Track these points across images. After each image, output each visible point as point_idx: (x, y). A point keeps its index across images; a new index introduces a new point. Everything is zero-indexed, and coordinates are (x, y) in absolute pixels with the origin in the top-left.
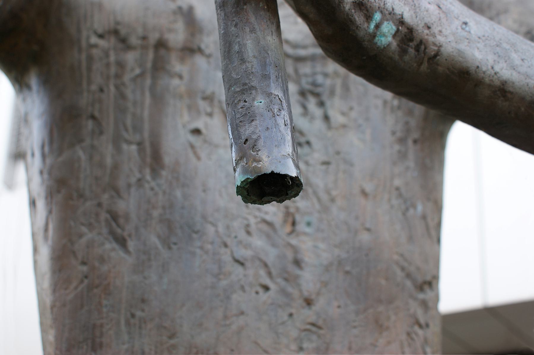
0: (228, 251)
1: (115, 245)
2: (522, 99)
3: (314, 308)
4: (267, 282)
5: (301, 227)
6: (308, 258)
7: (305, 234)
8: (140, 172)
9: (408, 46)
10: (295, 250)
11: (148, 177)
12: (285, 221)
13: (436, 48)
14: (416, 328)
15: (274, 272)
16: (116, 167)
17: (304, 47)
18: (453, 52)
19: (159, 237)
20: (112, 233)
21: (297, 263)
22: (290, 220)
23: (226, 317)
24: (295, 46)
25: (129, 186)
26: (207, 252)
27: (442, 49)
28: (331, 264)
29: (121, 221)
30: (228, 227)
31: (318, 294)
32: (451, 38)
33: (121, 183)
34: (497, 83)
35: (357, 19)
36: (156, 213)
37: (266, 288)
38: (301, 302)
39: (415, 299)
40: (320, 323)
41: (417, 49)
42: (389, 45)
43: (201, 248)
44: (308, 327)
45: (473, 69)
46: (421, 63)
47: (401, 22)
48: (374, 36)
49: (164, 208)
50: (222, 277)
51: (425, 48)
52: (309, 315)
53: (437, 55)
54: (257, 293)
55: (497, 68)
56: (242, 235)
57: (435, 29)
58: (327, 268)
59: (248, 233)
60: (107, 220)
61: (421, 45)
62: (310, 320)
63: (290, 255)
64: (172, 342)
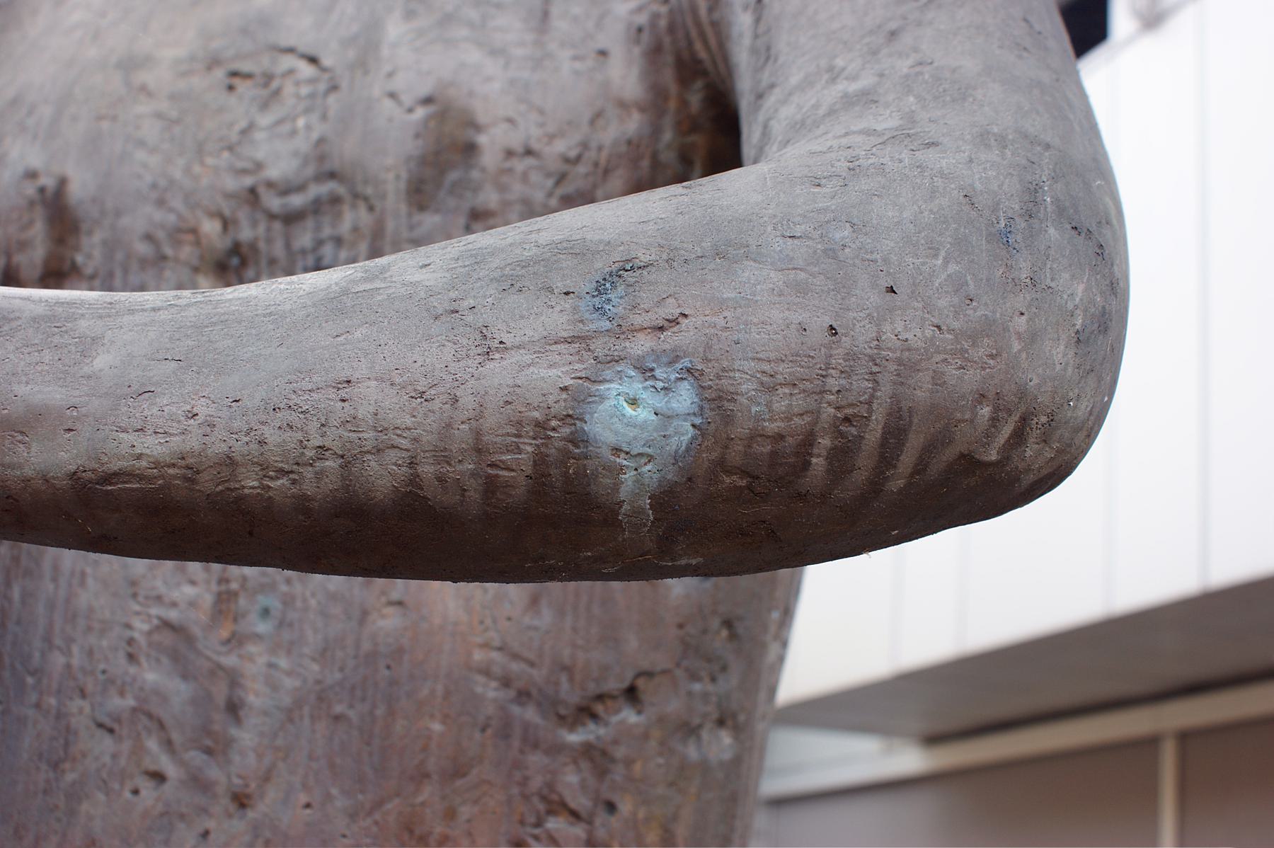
0: (86, 705)
3: (251, 814)
6: (256, 697)
7: (258, 637)
10: (234, 679)
15: (176, 736)
17: (301, 188)
22: (666, 324)
24: (286, 190)
28: (299, 704)
30: (90, 653)
31: (267, 778)
38: (225, 802)
43: (38, 706)
50: (67, 766)
54: (136, 792)
56: (120, 664)
58: (290, 715)
59: (131, 657)
63: (220, 692)
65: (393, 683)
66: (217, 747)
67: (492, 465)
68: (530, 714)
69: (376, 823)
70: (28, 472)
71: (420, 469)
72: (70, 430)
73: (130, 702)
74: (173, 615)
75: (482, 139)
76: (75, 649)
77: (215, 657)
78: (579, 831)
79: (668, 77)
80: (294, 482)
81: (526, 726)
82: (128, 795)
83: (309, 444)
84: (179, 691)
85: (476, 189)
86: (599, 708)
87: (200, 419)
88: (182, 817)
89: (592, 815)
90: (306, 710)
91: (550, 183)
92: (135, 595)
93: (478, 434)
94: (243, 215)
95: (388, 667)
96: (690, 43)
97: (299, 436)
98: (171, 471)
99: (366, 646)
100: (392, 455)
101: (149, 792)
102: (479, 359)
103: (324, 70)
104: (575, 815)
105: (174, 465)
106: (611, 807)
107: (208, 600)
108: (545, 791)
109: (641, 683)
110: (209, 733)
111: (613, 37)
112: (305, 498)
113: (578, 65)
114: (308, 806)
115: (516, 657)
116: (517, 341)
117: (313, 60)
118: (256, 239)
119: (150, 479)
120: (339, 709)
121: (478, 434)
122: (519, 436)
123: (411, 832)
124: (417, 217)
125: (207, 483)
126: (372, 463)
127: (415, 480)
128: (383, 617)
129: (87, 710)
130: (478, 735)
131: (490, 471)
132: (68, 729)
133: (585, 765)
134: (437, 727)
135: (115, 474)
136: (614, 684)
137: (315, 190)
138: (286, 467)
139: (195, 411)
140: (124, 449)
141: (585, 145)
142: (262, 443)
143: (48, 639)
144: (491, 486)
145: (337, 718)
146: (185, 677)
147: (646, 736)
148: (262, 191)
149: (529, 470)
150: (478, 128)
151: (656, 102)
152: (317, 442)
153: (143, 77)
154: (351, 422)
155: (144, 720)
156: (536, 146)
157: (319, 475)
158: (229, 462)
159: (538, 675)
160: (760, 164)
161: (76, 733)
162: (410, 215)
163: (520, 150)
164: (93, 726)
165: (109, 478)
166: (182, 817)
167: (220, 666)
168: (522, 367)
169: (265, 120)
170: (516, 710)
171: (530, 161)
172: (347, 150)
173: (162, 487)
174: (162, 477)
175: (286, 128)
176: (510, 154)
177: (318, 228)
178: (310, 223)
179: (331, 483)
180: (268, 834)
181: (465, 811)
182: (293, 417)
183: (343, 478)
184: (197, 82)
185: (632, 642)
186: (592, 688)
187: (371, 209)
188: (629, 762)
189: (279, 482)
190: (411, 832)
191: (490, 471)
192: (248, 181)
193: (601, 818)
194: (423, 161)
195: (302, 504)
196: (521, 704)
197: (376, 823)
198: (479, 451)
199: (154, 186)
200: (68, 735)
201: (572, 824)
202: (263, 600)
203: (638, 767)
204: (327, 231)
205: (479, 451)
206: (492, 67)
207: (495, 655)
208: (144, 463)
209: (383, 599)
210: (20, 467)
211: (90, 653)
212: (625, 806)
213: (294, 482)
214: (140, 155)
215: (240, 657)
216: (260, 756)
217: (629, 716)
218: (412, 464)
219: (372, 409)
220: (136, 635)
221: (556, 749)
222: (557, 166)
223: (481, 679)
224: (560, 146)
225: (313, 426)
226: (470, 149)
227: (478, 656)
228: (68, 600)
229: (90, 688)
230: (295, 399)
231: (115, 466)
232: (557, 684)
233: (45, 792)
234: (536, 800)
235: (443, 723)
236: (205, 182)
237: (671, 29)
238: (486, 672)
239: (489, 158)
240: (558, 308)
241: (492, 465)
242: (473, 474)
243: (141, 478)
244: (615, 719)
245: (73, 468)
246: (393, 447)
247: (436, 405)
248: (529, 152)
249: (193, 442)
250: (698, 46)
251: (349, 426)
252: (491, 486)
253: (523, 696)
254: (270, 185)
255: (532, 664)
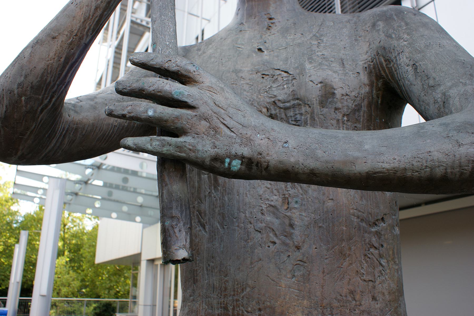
1: (201, 228)
2: (327, 175)
4: (275, 239)
5: (293, 205)
6: (297, 222)
8: (210, 189)
9: (252, 165)
10: (290, 219)
11: (213, 191)
12: (283, 203)
13: (266, 164)
14: (372, 250)
16: (199, 187)
17: (289, 102)
18: (276, 163)
19: (219, 223)
20: (199, 221)
21: (291, 226)
23: (252, 263)
25: (205, 196)
26: (241, 228)
27: (269, 163)
28: (310, 224)
29: (203, 215)
30: (251, 213)
32: (275, 156)
33: (202, 196)
34: (308, 171)
35: (216, 165)
36: (217, 210)
37: (274, 243)
38: (294, 248)
39: (370, 232)
40: (305, 259)
41: (257, 165)
42: (240, 169)
43: (238, 226)
44: (298, 262)
45: (290, 169)
46: (262, 172)
47: (242, 158)
48: (229, 168)
49: (220, 207)
50: (249, 241)
51: (261, 165)
52: (298, 255)
53: (268, 166)
54: (269, 247)
55: (305, 164)
57: (264, 154)
58: (308, 227)
60: (197, 215)
61: (258, 164)
62: (298, 259)
63: (287, 222)
64: (226, 278)
65: (333, 218)
66: (289, 235)
67: (463, 169)
68: (364, 224)
69: (333, 252)
70: (356, 172)
71: (447, 170)
72: (365, 162)
73: (264, 225)
74: (272, 203)
75: (336, 92)
76: (247, 212)
77: (284, 213)
78: (377, 252)
79: (374, 78)
80: (419, 173)
81: (364, 227)
82: (267, 247)
83: (423, 165)
84: (276, 222)
85: (336, 103)
86: (377, 223)
87: (397, 160)
88: (282, 252)
89: (379, 248)
90: (312, 225)
91: (352, 102)
92: (261, 199)
93: (460, 163)
94: (272, 107)
95: (331, 215)
96: (380, 71)
97: (421, 163)
98: (391, 171)
99: (325, 210)
100: (442, 168)
101: (272, 247)
102: (458, 147)
103: (290, 74)
104: (376, 248)
105: (392, 170)
106: (382, 246)
107: (280, 200)
108: (369, 243)
109: (384, 216)
110: (285, 232)
111: (360, 69)
112: (421, 177)
113: (354, 75)
114: (316, 248)
115: (360, 211)
116: (465, 143)
117: (286, 72)
118: (277, 113)
119: (385, 173)
120: (320, 225)
121: (460, 163)
122: (469, 163)
123: (342, 253)
124: (322, 109)
125: (399, 174)
126: (437, 169)
127: (446, 173)
128: (328, 202)
129: (253, 227)
130: (354, 230)
131: (462, 171)
132: (248, 231)
133: (376, 236)
134: (344, 228)
135: (377, 172)
136: (380, 217)
137: (292, 102)
138: (418, 170)
139: (395, 158)
140: (380, 167)
141: (359, 94)
142: (413, 165)
143: (239, 209)
144: (462, 174)
145: (320, 227)
146: (277, 218)
147: (387, 229)
148: (276, 102)
149: (470, 170)
150: (335, 89)
151: (371, 85)
152: (425, 165)
153: (240, 75)
154: (432, 160)
155: (268, 229)
156: (349, 94)
157: (425, 172)
158: (405, 169)
159: (365, 215)
160: (194, 88)
161: (250, 233)
162: (320, 109)
163: (345, 94)
164: (255, 231)
165: (375, 173)
166: (282, 252)
167: (286, 215)
168: (468, 149)
169: (275, 86)
170: (361, 224)
171: (348, 97)
172: (302, 93)
173: (388, 175)
174: (388, 173)
175: (281, 87)
176: (343, 95)
177: (295, 111)
178: (292, 110)
179: (427, 174)
180: (307, 255)
181: (353, 248)
182: (419, 159)
183: (431, 172)
184: (255, 76)
185: (382, 207)
186: (376, 218)
187: (310, 107)
188: (384, 235)
189: (416, 174)
190: (342, 253)
191: (462, 171)
192: (273, 100)
193: (381, 248)
194: (322, 96)
195: (420, 179)
196: (362, 222)
197: (333, 252)
198: (460, 166)
199: (250, 100)
200: (248, 233)
201: (375, 250)
202: (295, 199)
203: (386, 236)
204: (297, 112)
205: (460, 166)
206: (335, 75)
207: (355, 211)
208: (385, 170)
209: (328, 198)
210: (354, 171)
211: (251, 213)
212: (385, 245)
213: (419, 173)
214: (245, 93)
215: (291, 213)
216: (301, 237)
217: (382, 224)
218: (446, 169)
219: (437, 158)
220: (263, 208)
221: (370, 232)
222: (354, 98)
223: (353, 217)
224: (353, 94)
225: (424, 161)
226: (334, 94)
227: (351, 211)
228: (243, 200)
229: (252, 222)
230: (419, 156)
231: (378, 170)
232: (369, 217)
233: (244, 247)
234: (367, 244)
235: (346, 227)
236: (262, 100)
237: (374, 68)
238: (354, 215)
239: (338, 96)
240: (472, 136)
241: (463, 169)
242: (459, 172)
243: (383, 173)
244: (381, 225)
245: (367, 171)
246: (442, 166)
247: (451, 157)
248: (347, 95)
249: (396, 165)
250: (382, 72)
251: (432, 161)
252: (462, 174)
253: (362, 220)
254: (279, 100)
255: (363, 213)
